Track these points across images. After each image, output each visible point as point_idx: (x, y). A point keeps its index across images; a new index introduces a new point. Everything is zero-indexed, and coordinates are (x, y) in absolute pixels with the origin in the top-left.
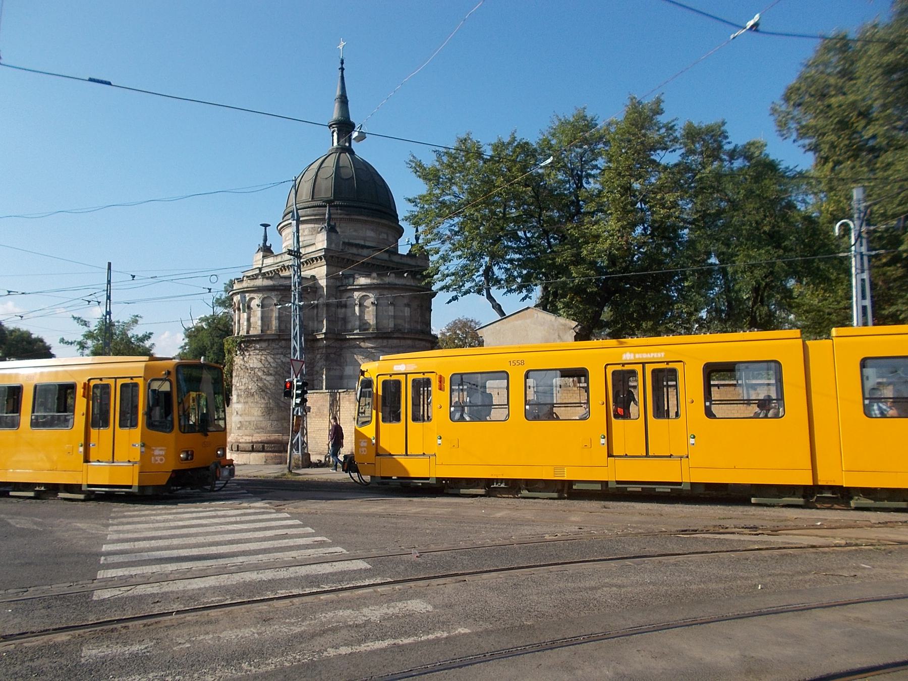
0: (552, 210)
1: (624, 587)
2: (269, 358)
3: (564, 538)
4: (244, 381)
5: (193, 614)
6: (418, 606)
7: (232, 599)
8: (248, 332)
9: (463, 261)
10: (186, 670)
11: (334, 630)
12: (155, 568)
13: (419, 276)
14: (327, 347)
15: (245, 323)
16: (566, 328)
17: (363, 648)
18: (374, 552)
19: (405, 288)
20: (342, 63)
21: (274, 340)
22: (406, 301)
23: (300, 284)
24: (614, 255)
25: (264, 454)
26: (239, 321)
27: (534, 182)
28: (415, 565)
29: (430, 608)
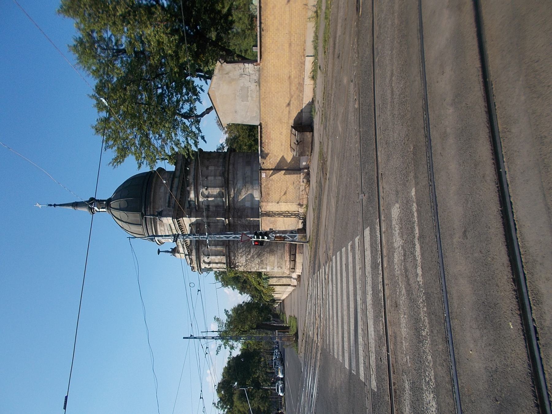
0: (142, 69)
1: (392, 70)
2: (240, 252)
3: (357, 94)
4: (253, 266)
5: (389, 343)
6: (395, 212)
7: (382, 317)
8: (224, 264)
9: (179, 132)
10: (423, 367)
11: (406, 270)
12: (361, 348)
13: (189, 160)
14: (233, 217)
15: (219, 265)
16: (221, 69)
17: (419, 258)
18: (360, 220)
19: (196, 169)
20: (51, 205)
21: (229, 250)
22: (205, 169)
23: (194, 235)
24: (171, 30)
25: (297, 255)
26: (217, 268)
27: (124, 81)
28: (370, 200)
29: (397, 205)
